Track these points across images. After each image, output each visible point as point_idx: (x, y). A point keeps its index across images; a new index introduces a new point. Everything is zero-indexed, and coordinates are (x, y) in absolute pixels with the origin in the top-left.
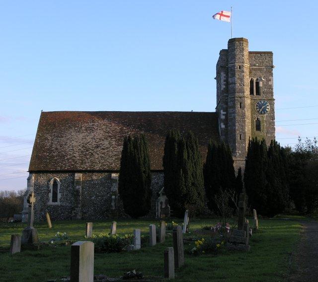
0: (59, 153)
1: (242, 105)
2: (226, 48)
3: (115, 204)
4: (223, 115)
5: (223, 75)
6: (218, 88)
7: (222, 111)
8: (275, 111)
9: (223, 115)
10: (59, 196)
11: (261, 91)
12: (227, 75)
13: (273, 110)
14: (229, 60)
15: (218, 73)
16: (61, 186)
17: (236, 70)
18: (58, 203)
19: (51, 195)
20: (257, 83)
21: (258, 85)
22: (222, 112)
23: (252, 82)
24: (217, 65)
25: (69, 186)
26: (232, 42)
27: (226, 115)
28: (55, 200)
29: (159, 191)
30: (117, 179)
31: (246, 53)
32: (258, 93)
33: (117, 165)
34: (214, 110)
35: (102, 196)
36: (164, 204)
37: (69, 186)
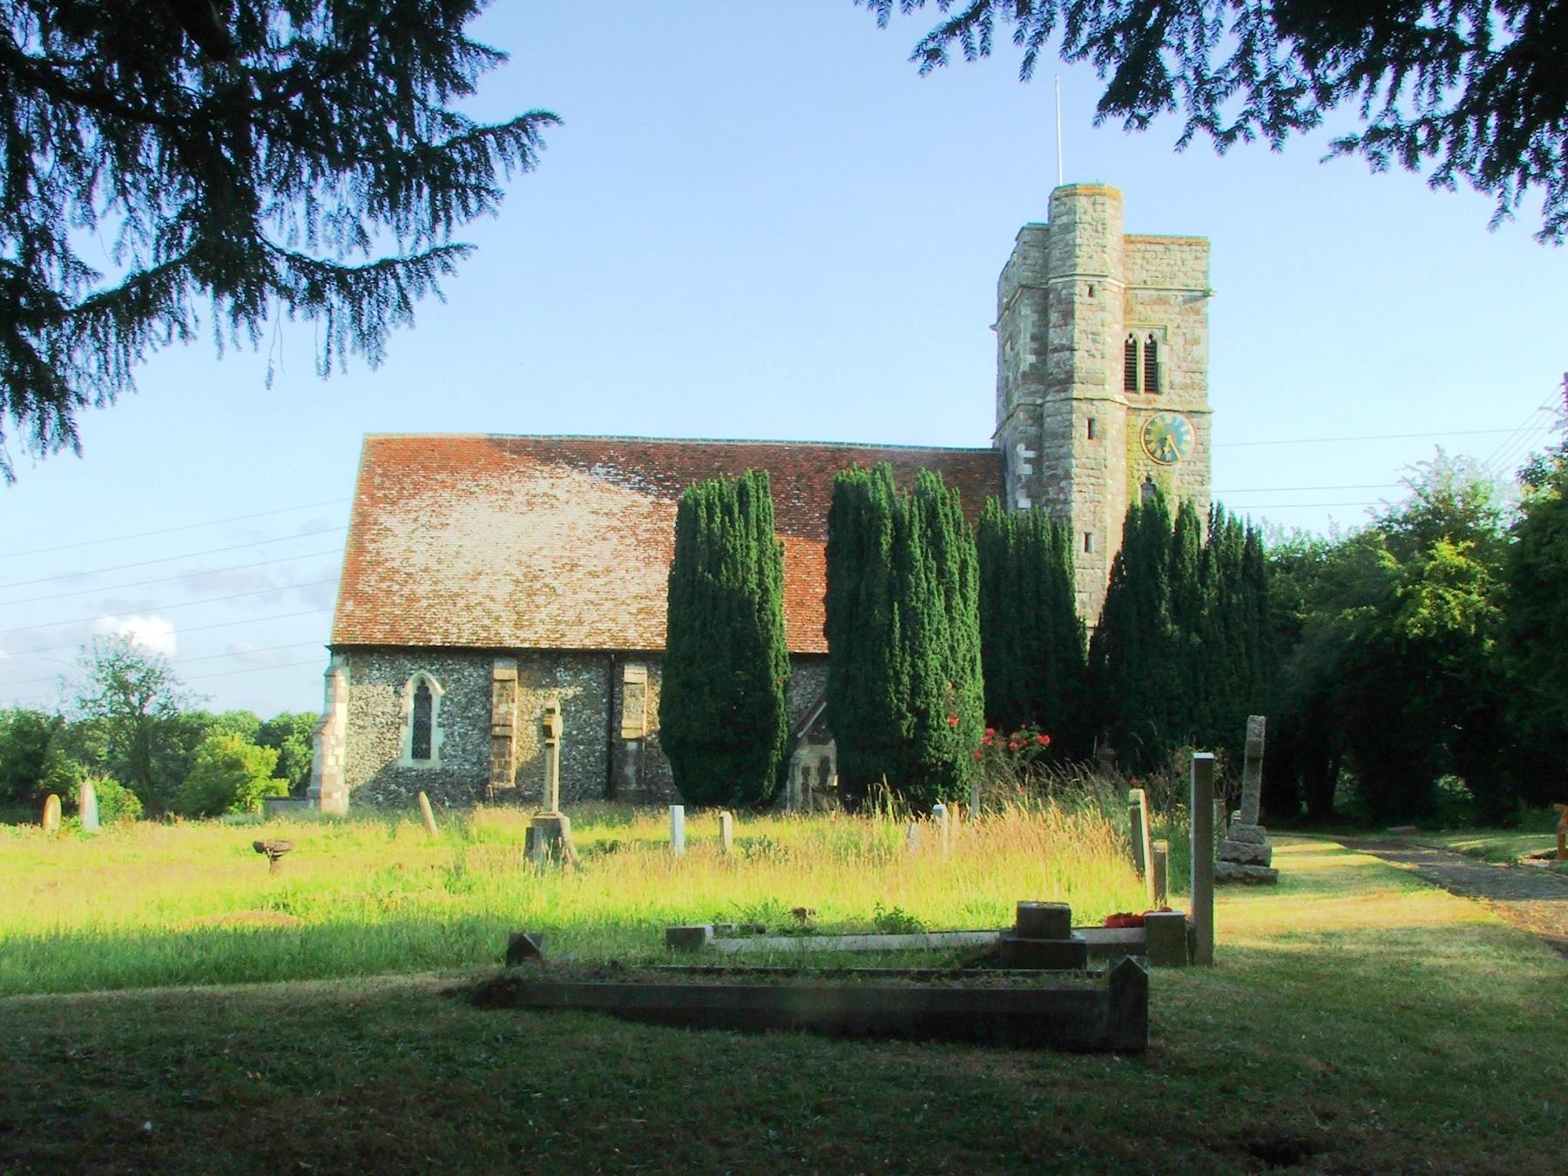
0: (436, 583)
1: (1097, 428)
2: (1042, 218)
3: (638, 771)
4: (1028, 461)
5: (1027, 315)
6: (1003, 362)
7: (1021, 449)
8: (1213, 451)
9: (1028, 461)
10: (437, 737)
11: (1165, 378)
12: (1043, 312)
13: (1202, 447)
14: (1054, 263)
15: (1007, 309)
16: (443, 704)
17: (1077, 299)
18: (434, 762)
19: (407, 732)
20: (1151, 349)
21: (1155, 356)
22: (1023, 452)
23: (1130, 349)
24: (1005, 276)
25: (471, 703)
26: (1063, 197)
27: (1036, 463)
28: (421, 750)
29: (800, 728)
30: (1088, 959)
31: (1113, 240)
32: (1153, 385)
33: (651, 632)
34: (988, 444)
35: (591, 743)
36: (813, 772)
37: (471, 703)
